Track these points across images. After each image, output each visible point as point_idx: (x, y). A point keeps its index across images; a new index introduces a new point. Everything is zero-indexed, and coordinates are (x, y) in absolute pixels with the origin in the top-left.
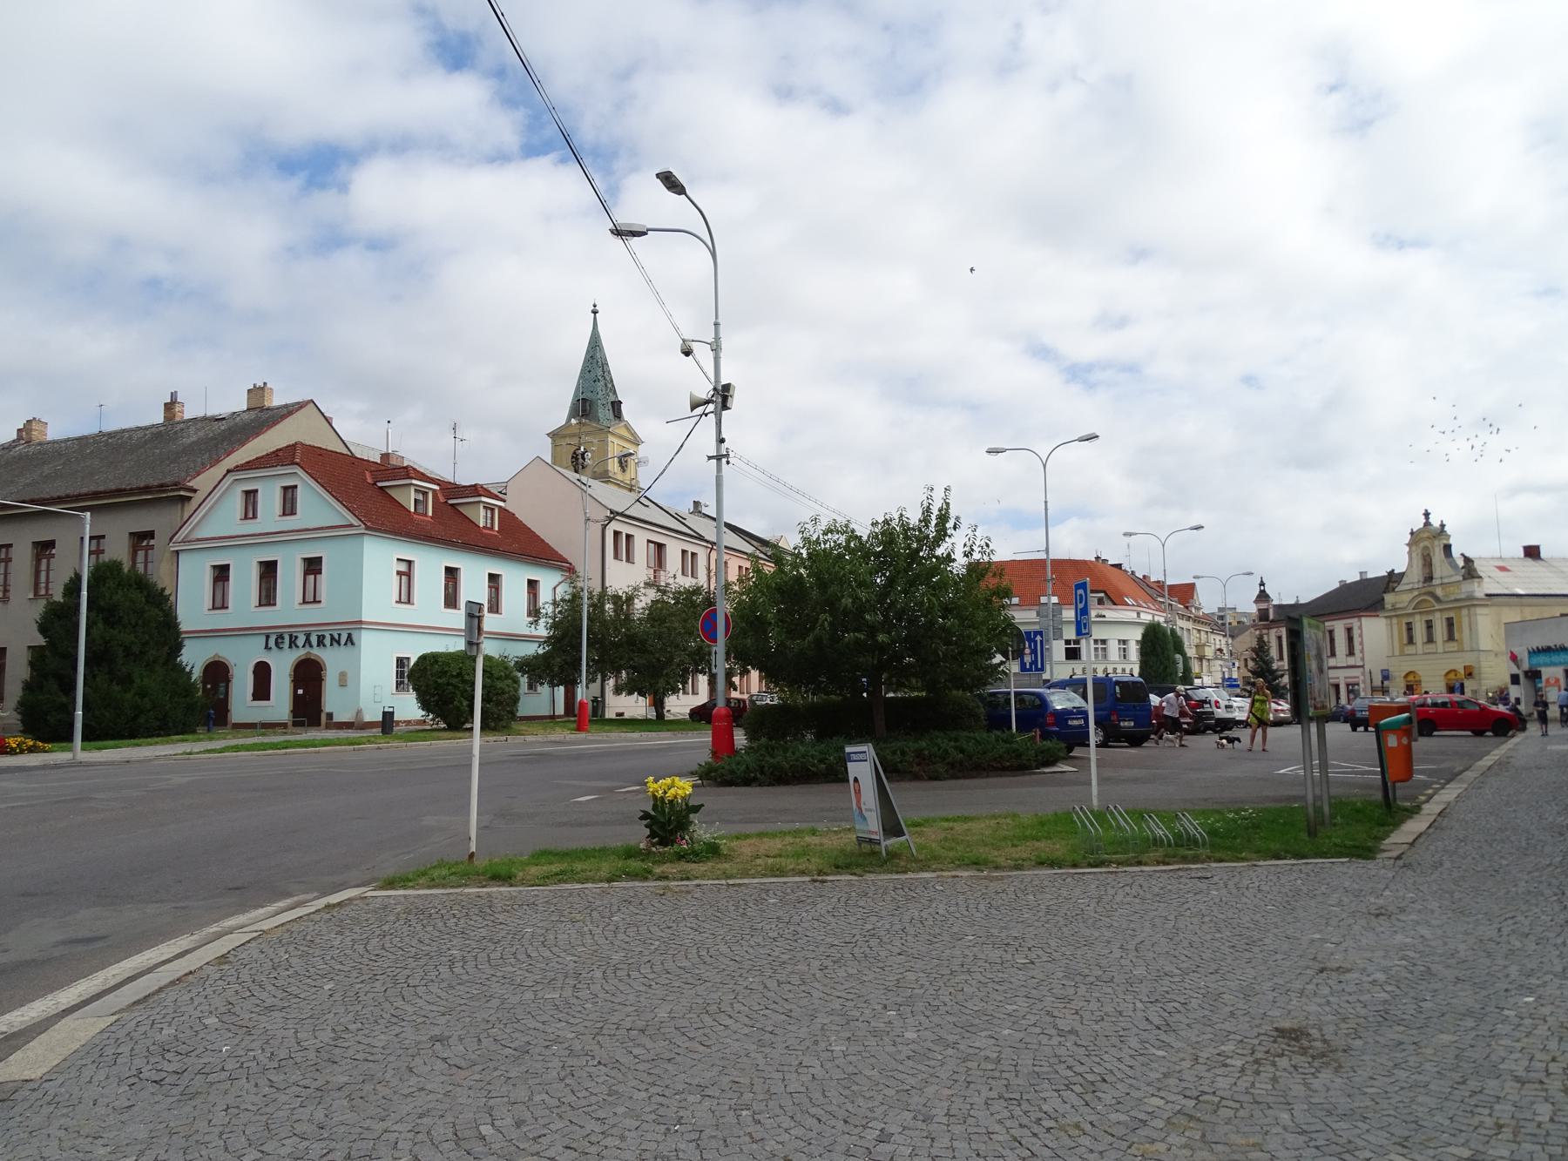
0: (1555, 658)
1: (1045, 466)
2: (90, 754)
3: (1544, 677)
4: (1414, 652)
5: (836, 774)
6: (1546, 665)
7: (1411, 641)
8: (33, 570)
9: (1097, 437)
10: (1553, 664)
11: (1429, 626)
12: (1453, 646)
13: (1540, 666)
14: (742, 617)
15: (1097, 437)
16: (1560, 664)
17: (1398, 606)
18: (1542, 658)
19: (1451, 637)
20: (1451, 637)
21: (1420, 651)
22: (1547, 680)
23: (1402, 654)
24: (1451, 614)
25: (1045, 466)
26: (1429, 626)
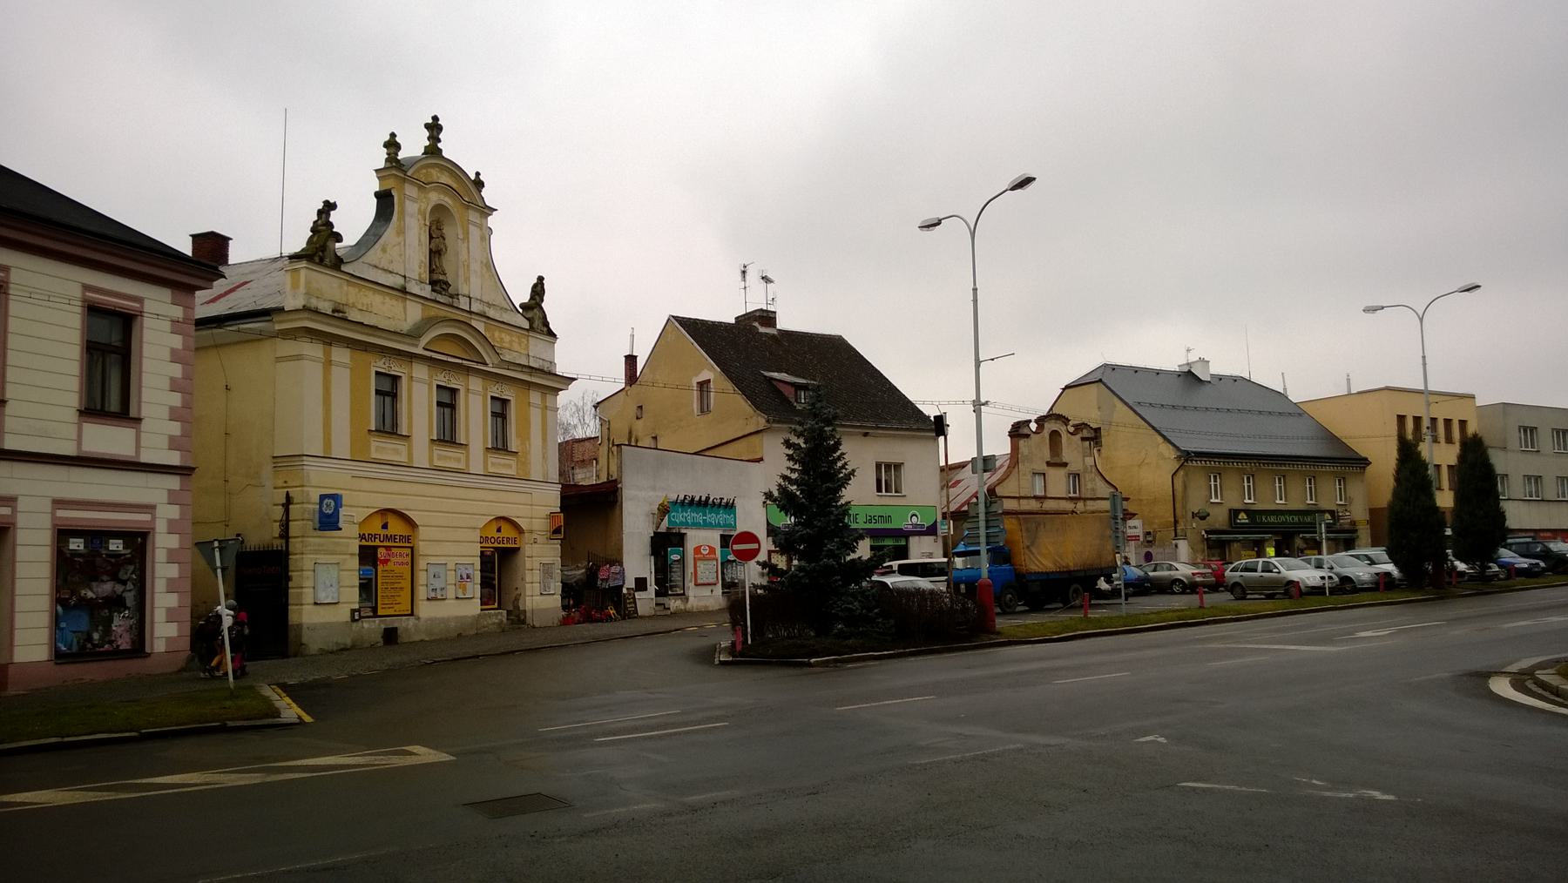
0: (712, 517)
1: (1421, 320)
3: (690, 545)
4: (403, 459)
6: (696, 526)
7: (389, 427)
8: (1483, 597)
9: (1479, 286)
10: (707, 526)
11: (448, 402)
12: (500, 464)
13: (687, 525)
14: (840, 344)
15: (1479, 286)
16: (718, 526)
17: (354, 315)
18: (679, 516)
19: (500, 446)
20: (500, 446)
21: (421, 458)
22: (697, 550)
23: (359, 457)
24: (507, 393)
25: (1421, 320)
26: (448, 402)
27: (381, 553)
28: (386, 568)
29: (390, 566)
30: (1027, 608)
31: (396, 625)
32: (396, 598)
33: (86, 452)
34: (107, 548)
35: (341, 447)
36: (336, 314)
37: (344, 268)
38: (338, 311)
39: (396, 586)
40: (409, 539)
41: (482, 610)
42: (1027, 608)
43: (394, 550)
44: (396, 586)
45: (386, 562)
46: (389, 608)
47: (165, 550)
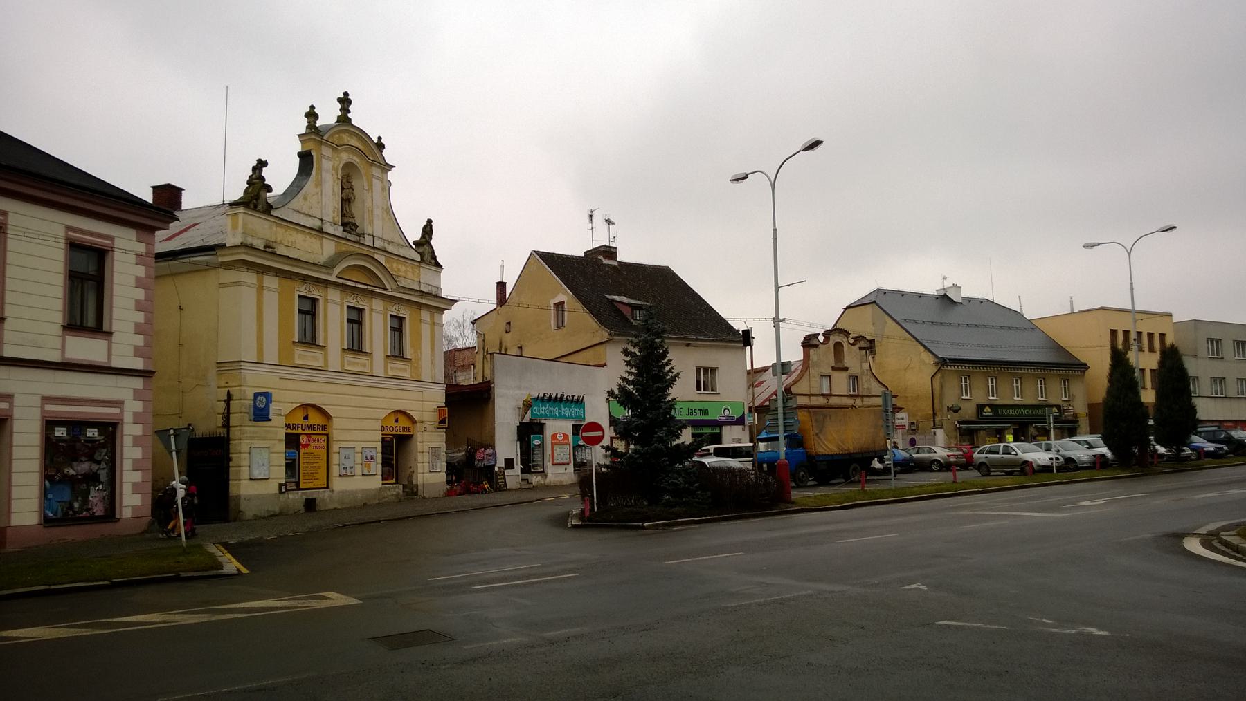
1: (1129, 254)
2: (321, 328)
3: (549, 433)
4: (320, 364)
5: (751, 442)
6: (553, 417)
7: (309, 339)
9: (1175, 227)
10: (562, 417)
11: (356, 319)
12: (397, 368)
13: (546, 417)
15: (1175, 227)
16: (571, 417)
17: (281, 250)
18: (540, 410)
19: (397, 354)
20: (397, 354)
21: (335, 364)
22: (554, 437)
23: (286, 363)
24: (403, 312)
25: (1129, 254)
26: (356, 319)
27: (303, 439)
28: (307, 451)
29: (310, 449)
30: (816, 483)
31: (314, 496)
32: (315, 475)
33: (68, 359)
34: (85, 435)
35: (271, 355)
36: (267, 250)
37: (273, 213)
38: (269, 247)
39: (315, 465)
40: (325, 428)
41: (383, 484)
42: (816, 483)
43: (313, 437)
44: (315, 465)
45: (307, 446)
46: (309, 483)
47: (131, 437)
